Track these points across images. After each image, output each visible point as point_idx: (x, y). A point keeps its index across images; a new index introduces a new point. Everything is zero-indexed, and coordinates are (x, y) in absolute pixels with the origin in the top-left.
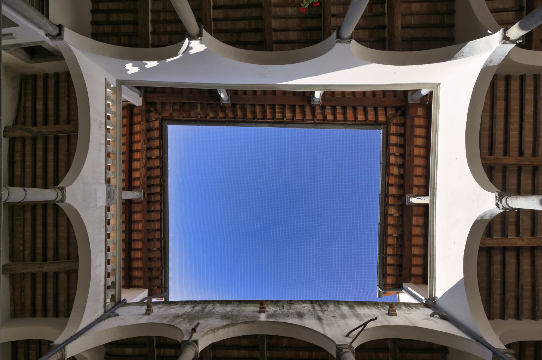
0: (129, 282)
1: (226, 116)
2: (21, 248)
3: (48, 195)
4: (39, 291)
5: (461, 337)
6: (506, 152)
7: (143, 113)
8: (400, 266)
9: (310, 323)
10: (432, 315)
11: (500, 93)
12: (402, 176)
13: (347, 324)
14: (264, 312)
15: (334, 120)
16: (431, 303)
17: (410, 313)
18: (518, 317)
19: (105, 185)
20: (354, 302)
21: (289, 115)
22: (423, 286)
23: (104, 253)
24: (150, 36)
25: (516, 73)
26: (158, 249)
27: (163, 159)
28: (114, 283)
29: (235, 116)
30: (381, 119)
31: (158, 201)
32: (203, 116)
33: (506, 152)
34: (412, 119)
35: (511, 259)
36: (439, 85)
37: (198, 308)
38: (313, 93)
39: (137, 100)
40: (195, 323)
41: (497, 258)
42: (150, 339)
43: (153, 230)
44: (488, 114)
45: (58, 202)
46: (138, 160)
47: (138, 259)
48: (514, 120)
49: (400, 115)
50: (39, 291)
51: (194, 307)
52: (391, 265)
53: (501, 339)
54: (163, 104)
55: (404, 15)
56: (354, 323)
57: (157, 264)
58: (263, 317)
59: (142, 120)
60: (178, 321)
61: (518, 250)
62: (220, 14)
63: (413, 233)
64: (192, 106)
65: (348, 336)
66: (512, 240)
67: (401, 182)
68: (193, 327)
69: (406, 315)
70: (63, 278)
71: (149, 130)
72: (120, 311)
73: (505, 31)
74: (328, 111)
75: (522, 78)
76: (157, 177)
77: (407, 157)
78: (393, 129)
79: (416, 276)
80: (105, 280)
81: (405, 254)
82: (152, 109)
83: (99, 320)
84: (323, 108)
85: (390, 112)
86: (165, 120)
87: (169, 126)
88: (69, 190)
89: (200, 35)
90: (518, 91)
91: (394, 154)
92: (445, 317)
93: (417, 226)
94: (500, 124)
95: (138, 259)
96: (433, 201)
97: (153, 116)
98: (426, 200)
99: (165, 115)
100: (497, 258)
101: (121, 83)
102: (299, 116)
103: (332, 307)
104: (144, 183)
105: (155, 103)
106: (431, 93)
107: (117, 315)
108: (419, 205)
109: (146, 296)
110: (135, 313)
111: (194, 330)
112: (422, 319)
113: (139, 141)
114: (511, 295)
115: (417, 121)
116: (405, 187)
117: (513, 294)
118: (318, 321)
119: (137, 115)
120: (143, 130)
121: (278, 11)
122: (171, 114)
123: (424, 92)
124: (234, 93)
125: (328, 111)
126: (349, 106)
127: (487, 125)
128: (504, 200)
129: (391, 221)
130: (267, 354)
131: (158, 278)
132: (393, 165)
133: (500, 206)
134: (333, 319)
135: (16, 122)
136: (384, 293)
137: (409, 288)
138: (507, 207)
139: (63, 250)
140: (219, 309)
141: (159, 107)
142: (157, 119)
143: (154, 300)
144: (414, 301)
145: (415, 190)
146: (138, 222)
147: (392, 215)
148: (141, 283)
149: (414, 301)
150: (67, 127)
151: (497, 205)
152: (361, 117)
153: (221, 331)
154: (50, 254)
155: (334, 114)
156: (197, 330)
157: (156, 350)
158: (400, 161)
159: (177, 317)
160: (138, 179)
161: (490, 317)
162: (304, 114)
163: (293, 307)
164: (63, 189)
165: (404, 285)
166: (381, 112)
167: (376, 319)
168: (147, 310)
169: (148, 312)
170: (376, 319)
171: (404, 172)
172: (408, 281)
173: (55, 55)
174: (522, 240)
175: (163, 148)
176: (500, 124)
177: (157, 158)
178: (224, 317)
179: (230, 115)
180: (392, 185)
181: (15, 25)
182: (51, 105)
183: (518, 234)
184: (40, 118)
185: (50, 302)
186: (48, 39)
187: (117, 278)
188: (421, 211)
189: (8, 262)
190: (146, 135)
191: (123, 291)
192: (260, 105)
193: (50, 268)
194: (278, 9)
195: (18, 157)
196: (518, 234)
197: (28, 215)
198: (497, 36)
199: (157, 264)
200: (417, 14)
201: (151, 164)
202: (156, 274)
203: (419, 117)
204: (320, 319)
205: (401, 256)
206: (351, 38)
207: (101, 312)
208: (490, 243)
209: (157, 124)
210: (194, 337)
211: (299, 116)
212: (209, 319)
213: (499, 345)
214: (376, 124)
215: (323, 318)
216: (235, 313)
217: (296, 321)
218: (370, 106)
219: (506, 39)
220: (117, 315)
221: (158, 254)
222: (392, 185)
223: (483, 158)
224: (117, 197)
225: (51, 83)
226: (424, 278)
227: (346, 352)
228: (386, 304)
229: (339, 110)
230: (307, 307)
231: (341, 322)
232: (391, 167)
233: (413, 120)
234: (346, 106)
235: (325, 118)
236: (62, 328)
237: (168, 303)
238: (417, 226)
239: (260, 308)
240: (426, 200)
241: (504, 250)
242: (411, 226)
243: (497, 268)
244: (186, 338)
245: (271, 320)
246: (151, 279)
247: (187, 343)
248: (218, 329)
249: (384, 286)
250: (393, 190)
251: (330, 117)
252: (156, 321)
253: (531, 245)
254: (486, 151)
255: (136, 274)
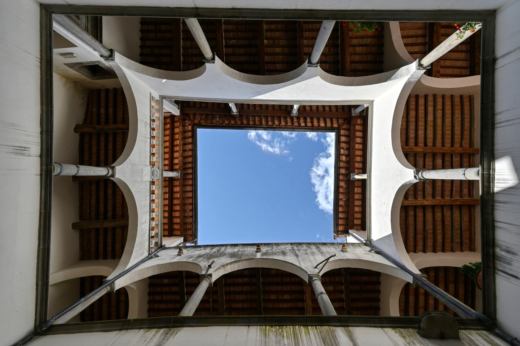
0: (170, 232)
1: (236, 122)
2: (88, 211)
3: (101, 171)
4: (101, 241)
5: (388, 266)
6: (416, 144)
7: (181, 121)
8: (347, 219)
9: (290, 259)
10: (370, 251)
11: (413, 107)
12: (347, 162)
13: (315, 259)
14: (260, 252)
15: (305, 126)
16: (369, 243)
17: (354, 251)
18: (424, 251)
19: (150, 166)
20: (320, 244)
21: (276, 123)
22: (361, 232)
23: (149, 213)
24: (182, 65)
25: (422, 93)
26: (190, 210)
27: (194, 151)
28: (157, 234)
29: (242, 123)
30: (335, 125)
31: (190, 179)
32: (221, 123)
33: (416, 144)
34: (355, 125)
35: (420, 214)
36: (373, 101)
37: (215, 250)
38: (292, 107)
39: (176, 111)
40: (211, 261)
41: (411, 213)
42: (181, 272)
43: (187, 198)
44: (405, 120)
45: (110, 177)
46: (177, 151)
47: (177, 217)
48: (421, 123)
49: (347, 124)
50: (101, 241)
51: (212, 249)
52: (341, 218)
53: (417, 266)
54: (194, 115)
55: (351, 54)
56: (320, 258)
57: (190, 220)
58: (259, 255)
59: (180, 125)
60: (200, 259)
61: (424, 207)
62: (230, 51)
63: (355, 198)
64: (213, 116)
65: (316, 267)
66: (420, 201)
67: (348, 166)
68: (209, 264)
69: (353, 252)
70: (119, 232)
71: (184, 132)
72: (161, 253)
73: (419, 61)
74: (302, 120)
75: (426, 97)
76: (190, 163)
77: (351, 150)
78: (342, 132)
79: (357, 225)
80: (150, 232)
81: (351, 210)
82: (187, 118)
83: (143, 261)
84: (298, 118)
85: (341, 121)
86: (196, 125)
87: (198, 129)
88: (118, 168)
89: (213, 59)
90: (424, 105)
91: (343, 148)
92: (379, 252)
93: (357, 193)
94: (412, 127)
95: (177, 217)
96: (370, 177)
97: (187, 122)
98: (364, 177)
99: (196, 122)
100: (411, 213)
101: (163, 97)
102: (283, 123)
103: (305, 247)
104: (181, 167)
105: (189, 114)
106: (367, 108)
107: (158, 256)
108: (359, 180)
109: (182, 241)
110: (172, 255)
111: (210, 266)
112: (363, 254)
113: (178, 139)
114: (420, 237)
115: (358, 127)
116: (350, 169)
117: (421, 236)
118: (296, 257)
119: (177, 122)
120: (181, 132)
121: (269, 50)
122: (200, 121)
123: (365, 106)
124: (240, 106)
125: (302, 120)
126: (315, 117)
127: (404, 127)
128: (420, 174)
129: (341, 190)
130: (261, 280)
131: (190, 229)
132: (342, 155)
133: (418, 178)
134: (306, 255)
135: (85, 121)
136: (337, 236)
137: (354, 234)
138: (422, 178)
139: (119, 211)
140: (229, 250)
141: (191, 117)
142: (190, 125)
143: (188, 244)
144: (358, 242)
145: (356, 171)
146: (177, 192)
147: (342, 187)
148: (179, 233)
149: (358, 242)
150: (122, 126)
151: (415, 177)
152: (322, 125)
153: (229, 266)
154: (110, 214)
155: (305, 122)
156: (212, 266)
157: (185, 280)
158: (346, 152)
159: (200, 256)
160: (177, 164)
161: (408, 252)
162: (286, 122)
163: (279, 247)
164: (113, 168)
165: (350, 231)
166: (335, 121)
167: (335, 255)
168: (179, 252)
169: (179, 254)
170: (335, 255)
171: (350, 159)
172: (352, 228)
173: (110, 73)
174: (427, 201)
175: (194, 143)
176: (412, 127)
177: (190, 150)
178: (232, 255)
179: (239, 123)
180: (342, 168)
181: (75, 46)
182: (111, 110)
183: (424, 197)
184: (103, 120)
185: (109, 248)
186: (102, 60)
187: (158, 230)
188: (360, 184)
189: (78, 221)
190: (183, 135)
191: (163, 238)
192: (258, 116)
193: (109, 224)
194: (269, 49)
195: (86, 147)
196: (424, 197)
197: (94, 188)
198: (414, 65)
199: (190, 220)
200: (359, 54)
201: (186, 154)
202: (189, 226)
203: (358, 125)
204: (297, 256)
205: (348, 212)
206: (318, 63)
207: (146, 254)
208: (407, 203)
209: (190, 128)
210: (209, 272)
211: (283, 123)
212: (222, 258)
213: (417, 272)
214: (331, 129)
215: (299, 255)
216: (240, 253)
217: (281, 258)
218: (328, 118)
219: (420, 65)
220: (158, 256)
221: (190, 214)
222: (342, 168)
223: (403, 148)
224: (159, 174)
225: (111, 95)
226: (363, 225)
227: (315, 280)
228: (340, 244)
229: (309, 120)
230: (289, 247)
231: (311, 258)
232: (341, 156)
233: (355, 127)
234: (314, 116)
235: (300, 124)
236: (114, 267)
237: (196, 247)
238: (357, 193)
239: (257, 249)
240: (364, 177)
241: (415, 207)
242: (354, 193)
243: (411, 219)
244: (204, 273)
245: (264, 257)
246: (186, 230)
247: (204, 276)
248: (227, 264)
249: (337, 232)
250: (343, 171)
251: (303, 124)
252: (184, 260)
253: (432, 204)
254: (404, 144)
255: (176, 227)
